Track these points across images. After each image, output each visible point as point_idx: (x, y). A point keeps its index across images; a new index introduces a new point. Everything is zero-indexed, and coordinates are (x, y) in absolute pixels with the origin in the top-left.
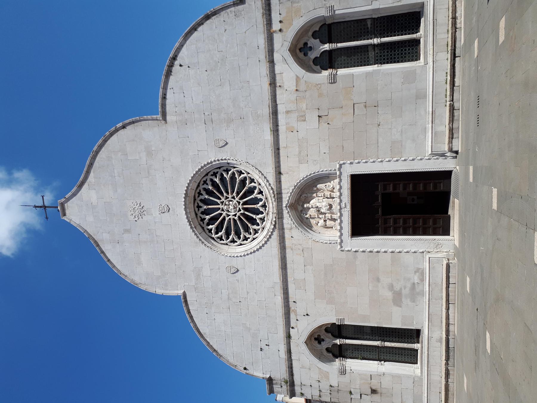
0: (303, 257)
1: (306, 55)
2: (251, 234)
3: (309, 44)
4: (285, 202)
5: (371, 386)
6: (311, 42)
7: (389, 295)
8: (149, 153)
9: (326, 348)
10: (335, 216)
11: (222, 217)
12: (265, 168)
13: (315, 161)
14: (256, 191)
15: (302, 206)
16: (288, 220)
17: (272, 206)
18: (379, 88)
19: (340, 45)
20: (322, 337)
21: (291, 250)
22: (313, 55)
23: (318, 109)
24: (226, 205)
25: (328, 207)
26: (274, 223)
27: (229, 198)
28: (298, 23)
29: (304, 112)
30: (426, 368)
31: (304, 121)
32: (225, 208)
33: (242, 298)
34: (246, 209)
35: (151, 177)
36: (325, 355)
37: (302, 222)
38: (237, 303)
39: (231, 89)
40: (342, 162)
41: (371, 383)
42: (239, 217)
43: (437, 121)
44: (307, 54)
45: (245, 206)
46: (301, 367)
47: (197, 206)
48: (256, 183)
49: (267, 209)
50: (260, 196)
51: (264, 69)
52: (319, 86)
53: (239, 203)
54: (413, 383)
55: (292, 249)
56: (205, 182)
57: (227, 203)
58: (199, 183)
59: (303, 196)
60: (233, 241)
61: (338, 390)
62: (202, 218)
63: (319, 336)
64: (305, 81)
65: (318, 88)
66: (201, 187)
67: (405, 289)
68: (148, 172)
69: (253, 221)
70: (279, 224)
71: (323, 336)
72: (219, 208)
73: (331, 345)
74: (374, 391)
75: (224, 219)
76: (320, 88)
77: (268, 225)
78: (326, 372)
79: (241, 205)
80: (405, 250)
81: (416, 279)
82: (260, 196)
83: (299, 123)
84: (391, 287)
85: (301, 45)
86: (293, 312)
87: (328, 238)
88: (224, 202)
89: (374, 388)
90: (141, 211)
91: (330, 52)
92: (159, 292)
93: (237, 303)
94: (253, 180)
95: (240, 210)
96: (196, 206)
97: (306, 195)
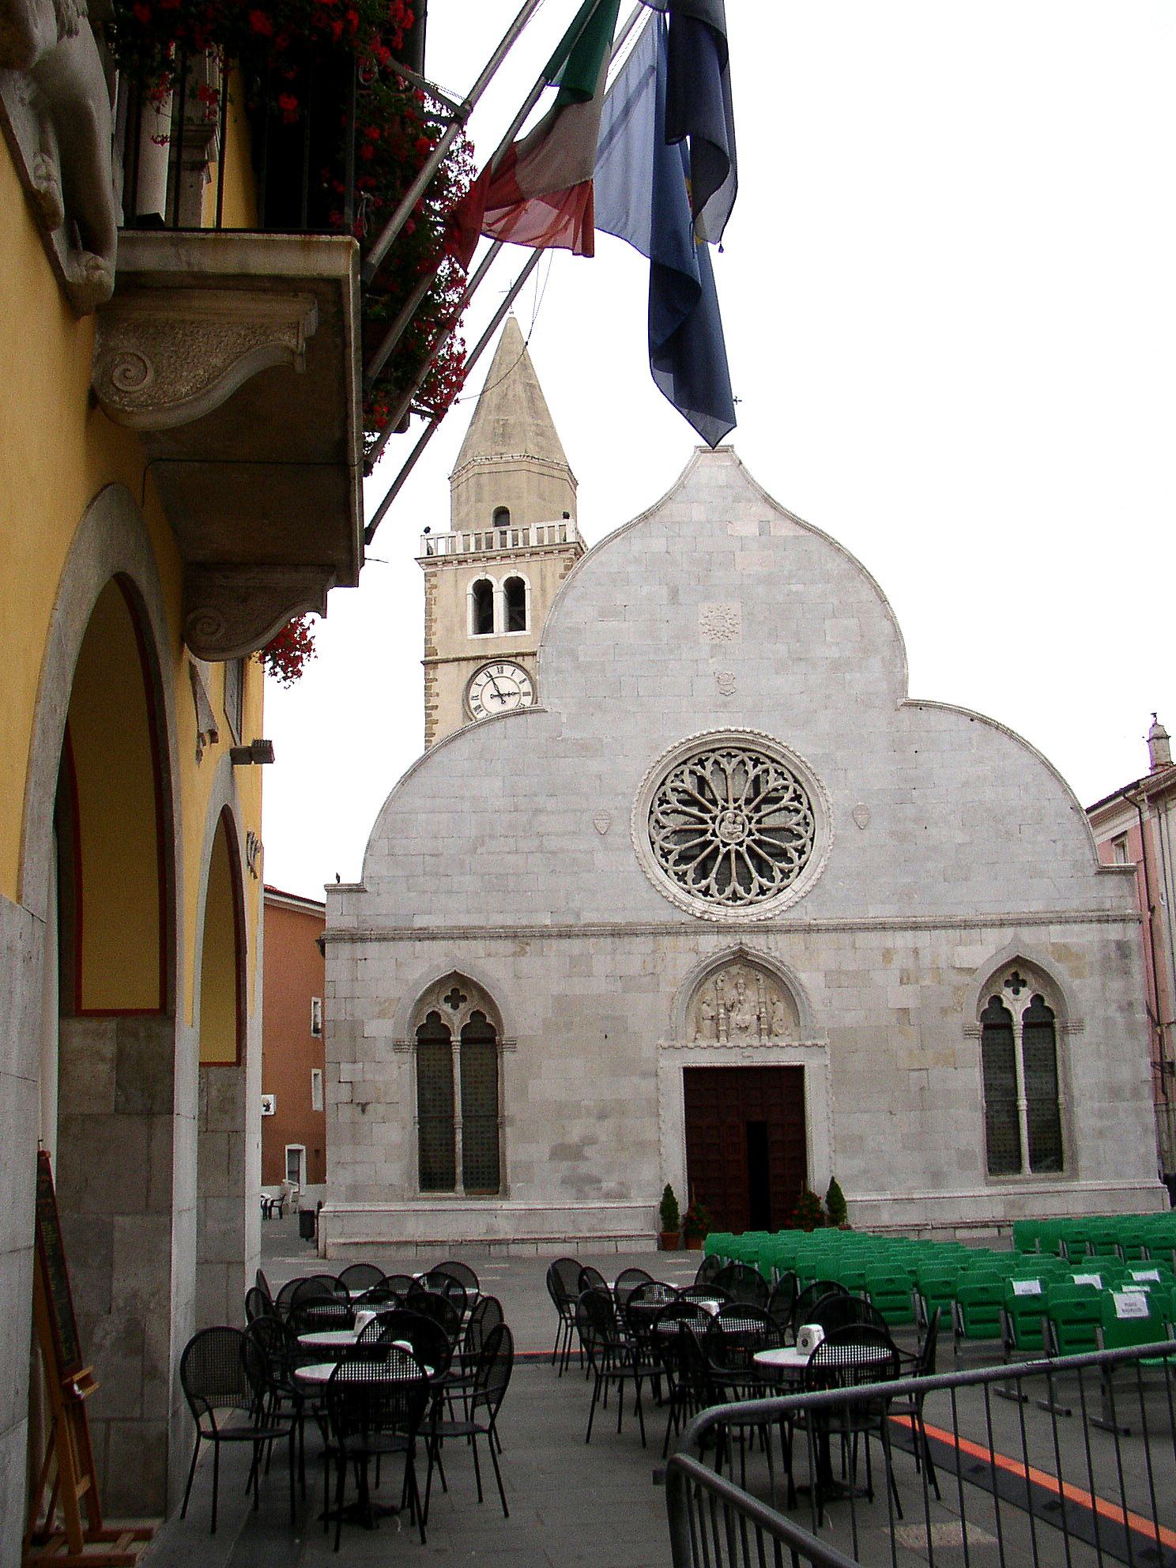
1: (1007, 984)
2: (675, 865)
4: (746, 939)
7: (575, 1135)
11: (710, 806)
14: (764, 881)
16: (712, 945)
18: (952, 1110)
19: (1019, 1043)
20: (462, 1005)
25: (743, 1026)
26: (706, 917)
28: (1059, 971)
29: (917, 982)
30: (427, 1207)
32: (729, 814)
34: (727, 855)
35: (790, 663)
43: (897, 1207)
45: (733, 856)
49: (730, 903)
51: (992, 911)
53: (740, 844)
55: (654, 952)
56: (757, 762)
57: (739, 819)
69: (703, 872)
70: (704, 926)
81: (609, 1184)
82: (755, 888)
83: (897, 973)
84: (591, 1141)
91: (1008, 1027)
95: (725, 845)
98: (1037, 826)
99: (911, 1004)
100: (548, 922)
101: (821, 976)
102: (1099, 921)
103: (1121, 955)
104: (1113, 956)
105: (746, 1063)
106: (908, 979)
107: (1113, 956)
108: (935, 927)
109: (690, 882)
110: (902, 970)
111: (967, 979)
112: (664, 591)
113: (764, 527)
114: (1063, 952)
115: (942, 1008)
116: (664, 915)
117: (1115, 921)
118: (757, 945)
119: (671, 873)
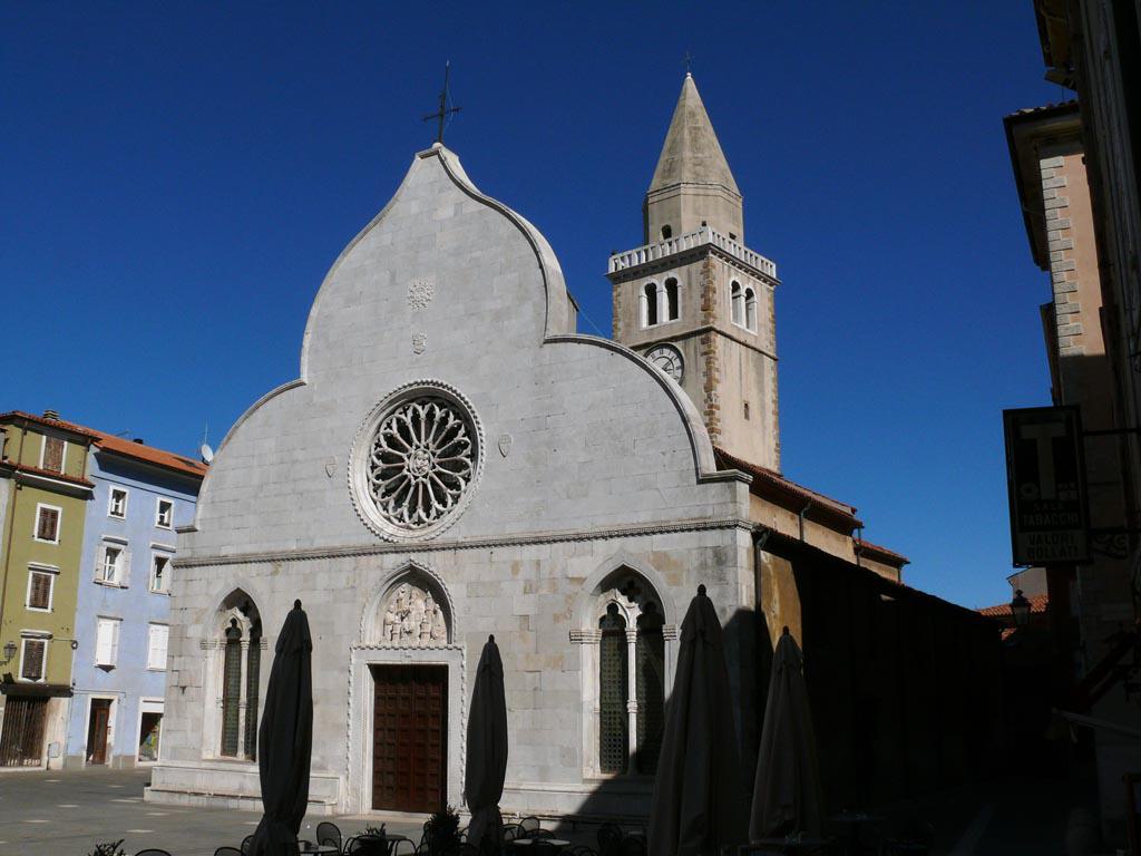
4: (413, 556)
8: (498, 316)
10: (397, 638)
16: (393, 562)
17: (418, 536)
29: (537, 591)
34: (417, 485)
40: (465, 652)
42: (406, 476)
50: (450, 501)
51: (603, 524)
55: (355, 569)
60: (374, 467)
68: (473, 315)
72: (407, 451)
75: (405, 450)
77: (390, 529)
80: (350, 745)
83: (522, 583)
87: (368, 627)
92: (314, 312)
95: (416, 478)
98: (649, 440)
99: (531, 611)
100: (294, 548)
101: (464, 586)
102: (698, 529)
103: (717, 562)
104: (710, 562)
105: (406, 662)
106: (531, 589)
107: (710, 562)
108: (555, 541)
109: (426, 519)
110: (527, 581)
111: (576, 588)
112: (387, 276)
113: (458, 206)
114: (661, 560)
115: (555, 615)
116: (367, 540)
117: (713, 528)
118: (422, 560)
119: (378, 504)
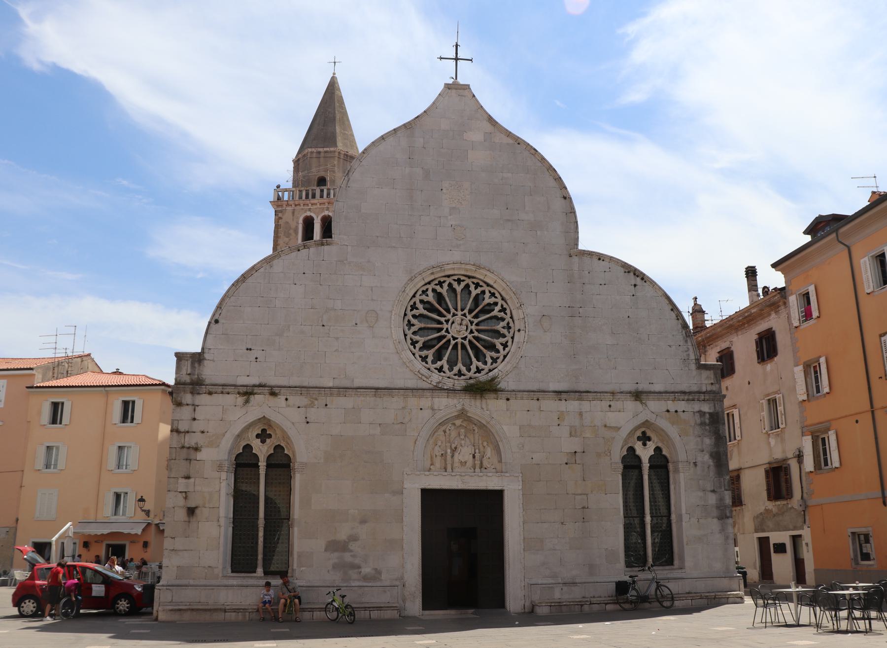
0: (393, 423)
1: (639, 439)
3: (650, 442)
5: (199, 507)
6: (652, 445)
7: (342, 536)
9: (252, 445)
12: (514, 380)
13: (523, 446)
15: (461, 425)
20: (268, 441)
21: (403, 407)
22: (638, 447)
23: (584, 452)
24: (462, 320)
27: (472, 325)
31: (570, 434)
33: (329, 330)
36: (241, 443)
37: (440, 424)
38: (322, 321)
39: (608, 346)
41: (205, 507)
44: (640, 441)
46: (224, 407)
47: (506, 310)
48: (491, 365)
52: (609, 454)
54: (209, 567)
55: (403, 408)
58: (492, 287)
59: (476, 428)
61: (190, 460)
62: (443, 284)
63: (270, 436)
64: (614, 438)
65: (606, 453)
66: (487, 289)
67: (351, 556)
68: (509, 220)
71: (270, 443)
73: (256, 453)
74: (191, 511)
76: (607, 455)
78: (220, 443)
79: (450, 339)
83: (568, 428)
84: (354, 538)
85: (649, 433)
86: (310, 402)
88: (466, 317)
89: (198, 511)
90: (455, 200)
93: (322, 321)
94: (496, 362)
96: (460, 277)
97: (476, 431)
119: (417, 356)
